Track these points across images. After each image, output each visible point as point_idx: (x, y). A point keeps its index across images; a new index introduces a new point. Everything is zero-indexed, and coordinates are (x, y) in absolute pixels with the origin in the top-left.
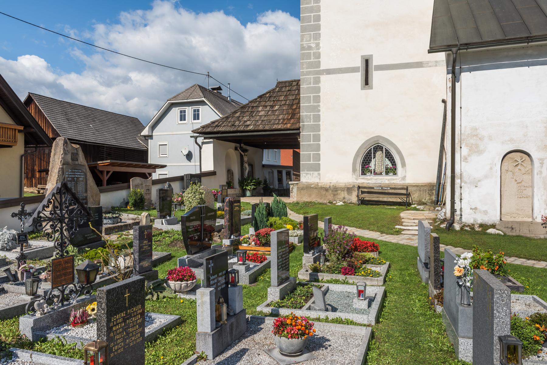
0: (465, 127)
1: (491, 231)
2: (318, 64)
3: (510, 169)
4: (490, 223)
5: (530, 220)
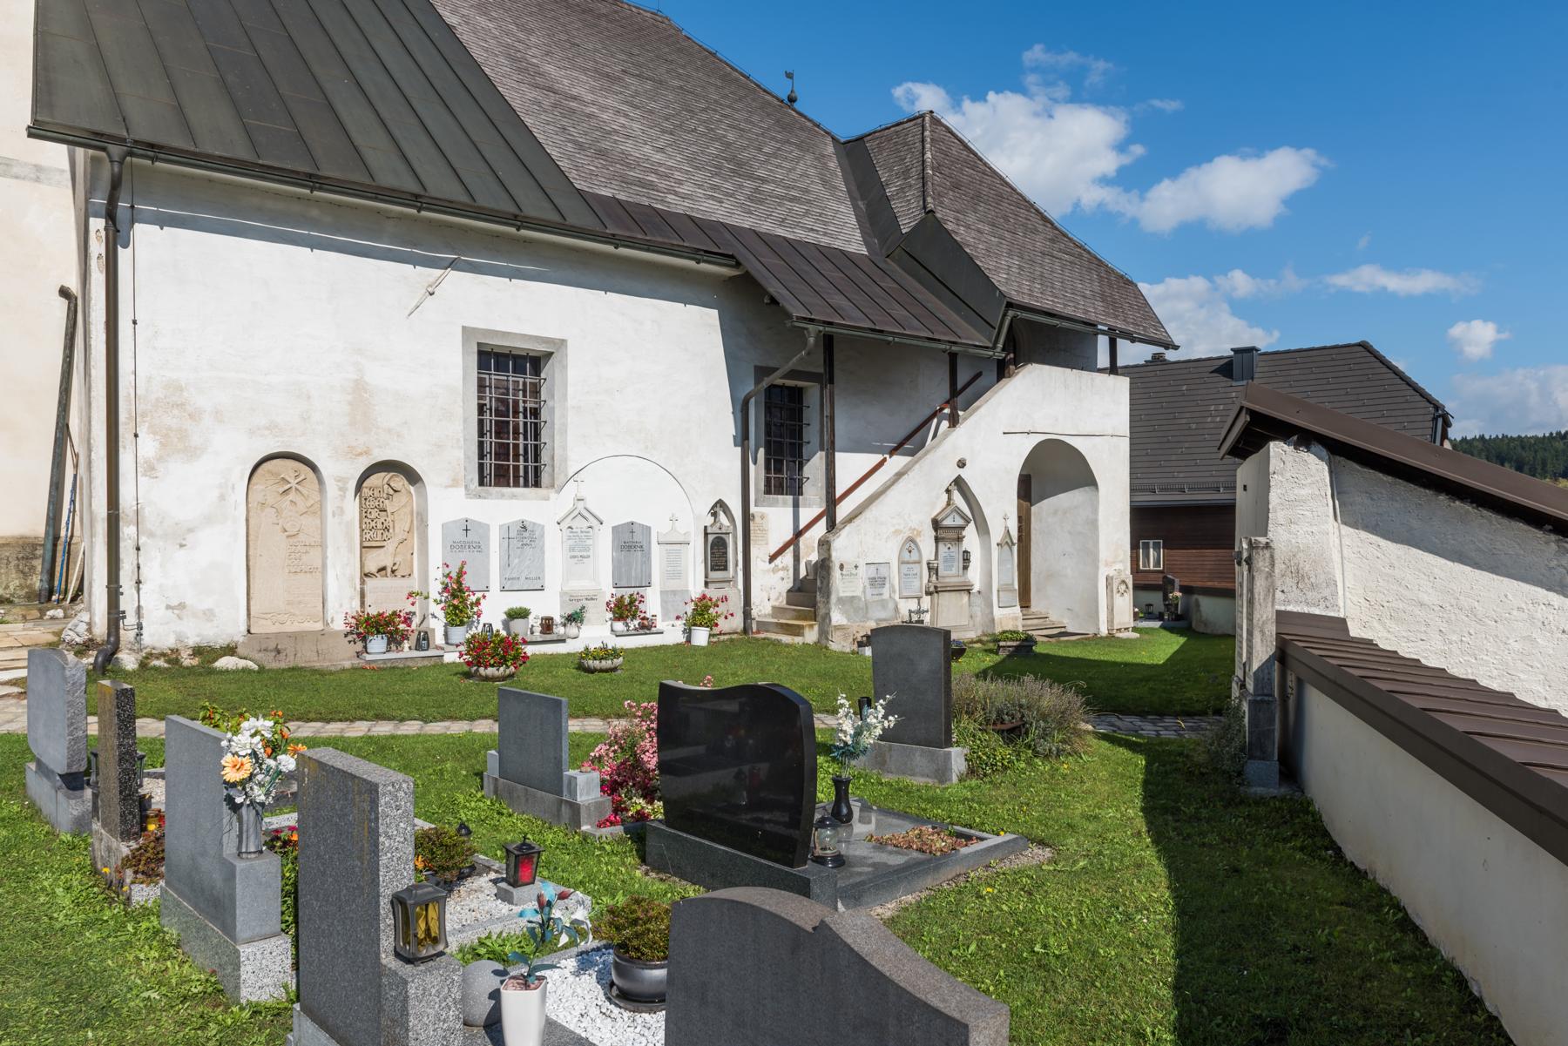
0: (149, 379)
1: (225, 662)
3: (270, 500)
4: (221, 641)
5: (319, 626)
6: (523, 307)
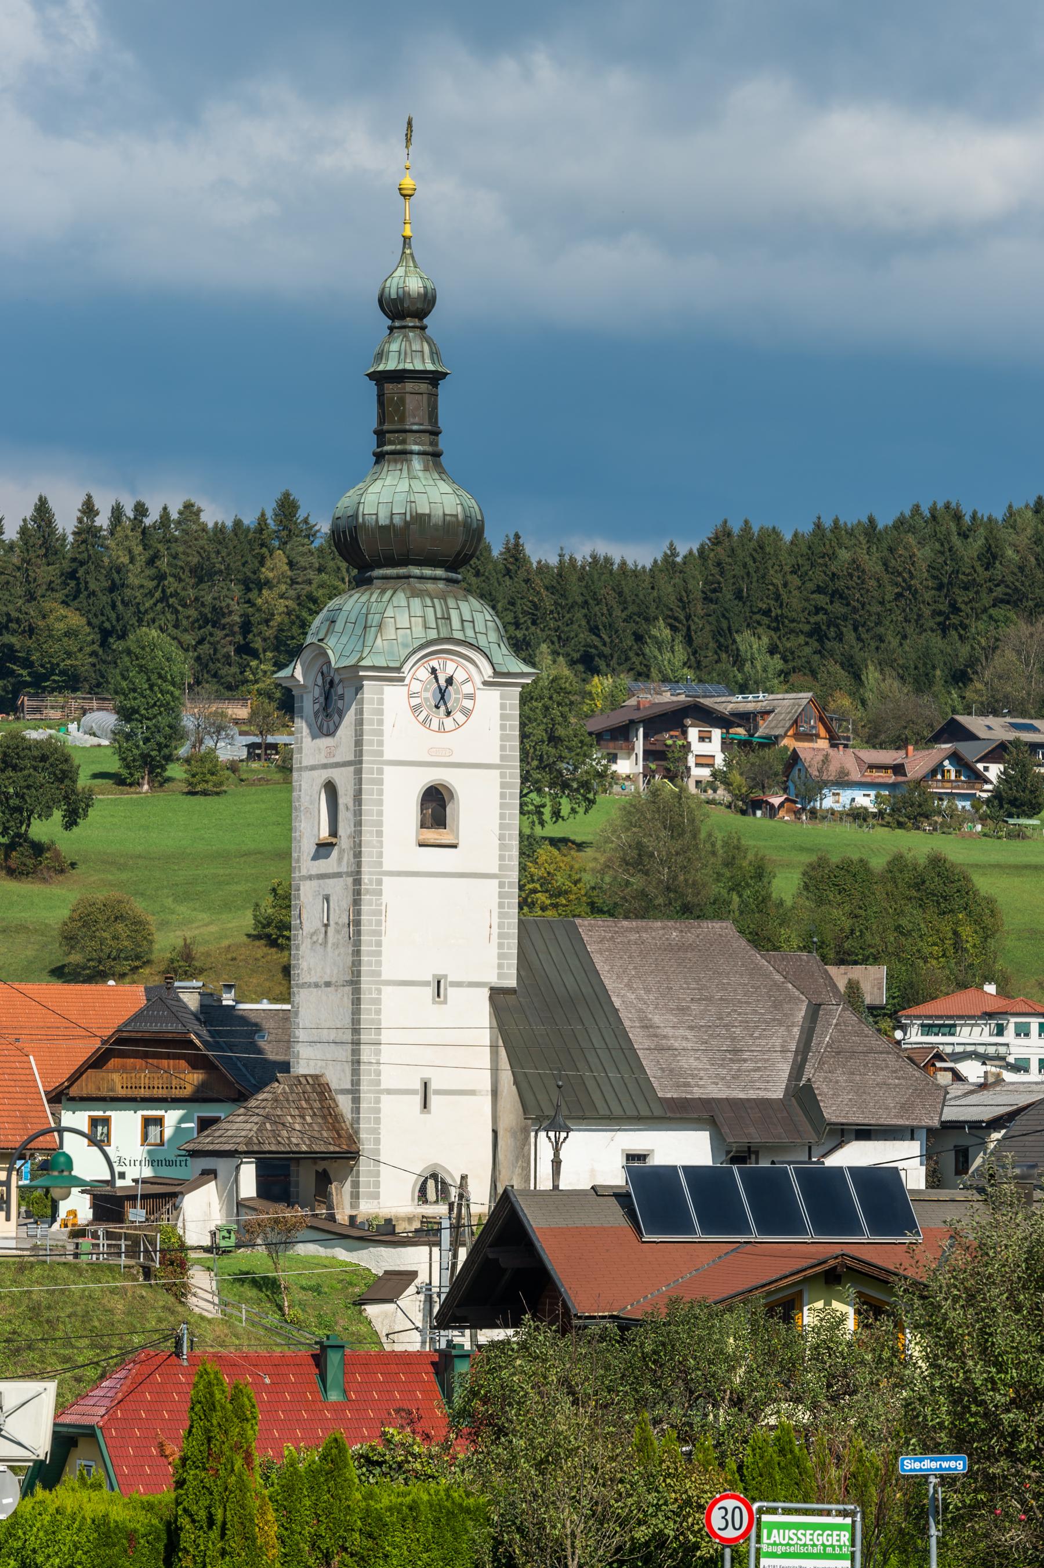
2: (378, 1083)
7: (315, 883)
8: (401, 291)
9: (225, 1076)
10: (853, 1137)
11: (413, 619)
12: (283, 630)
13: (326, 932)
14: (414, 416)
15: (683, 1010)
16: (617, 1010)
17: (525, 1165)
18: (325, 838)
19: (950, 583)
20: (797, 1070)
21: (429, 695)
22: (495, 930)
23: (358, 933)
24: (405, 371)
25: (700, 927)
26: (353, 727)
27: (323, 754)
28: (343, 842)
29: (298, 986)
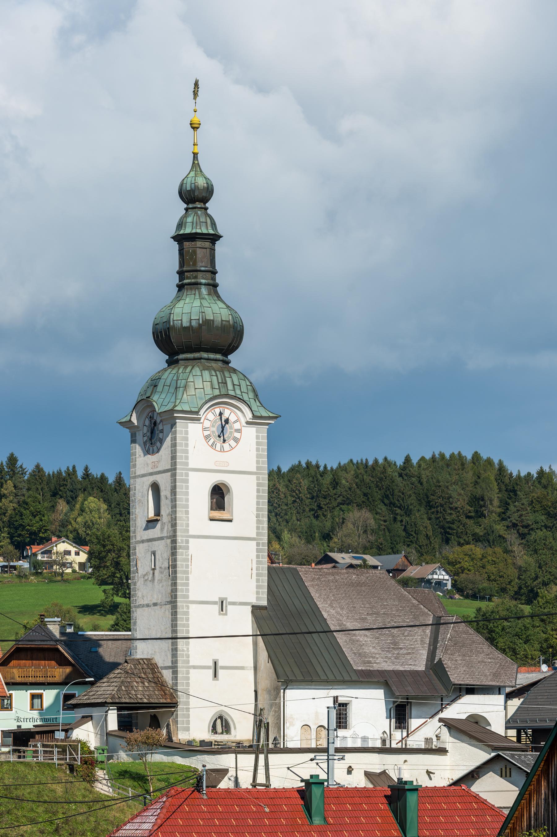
2: (188, 662)
6: (345, 694)
7: (146, 544)
8: (193, 185)
9: (78, 670)
10: (465, 693)
11: (205, 383)
12: (12, 518)
13: (153, 573)
14: (202, 262)
15: (363, 619)
16: (325, 619)
17: (277, 709)
18: (152, 517)
19: (317, 496)
20: (432, 654)
21: (214, 429)
22: (254, 571)
23: (175, 572)
24: (196, 234)
25: (368, 573)
26: (170, 449)
27: (150, 466)
28: (164, 518)
29: (135, 607)
